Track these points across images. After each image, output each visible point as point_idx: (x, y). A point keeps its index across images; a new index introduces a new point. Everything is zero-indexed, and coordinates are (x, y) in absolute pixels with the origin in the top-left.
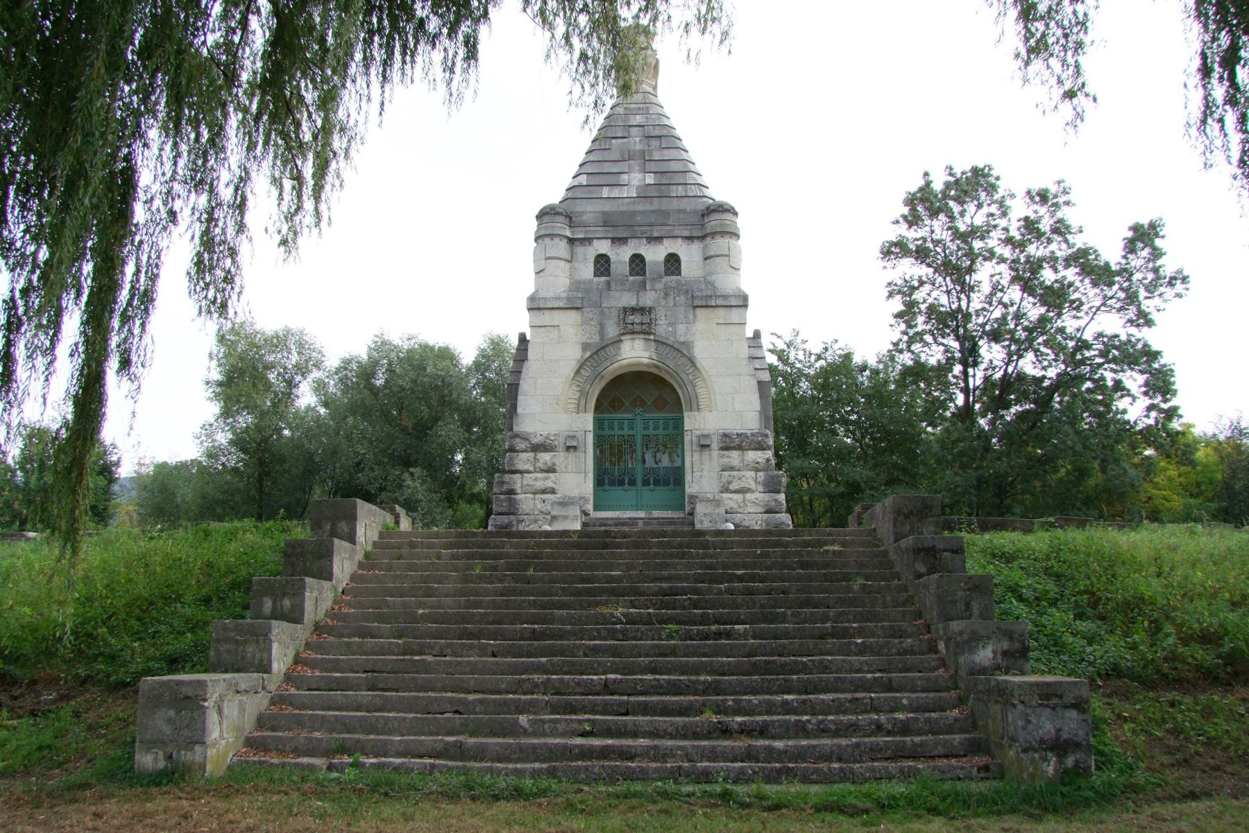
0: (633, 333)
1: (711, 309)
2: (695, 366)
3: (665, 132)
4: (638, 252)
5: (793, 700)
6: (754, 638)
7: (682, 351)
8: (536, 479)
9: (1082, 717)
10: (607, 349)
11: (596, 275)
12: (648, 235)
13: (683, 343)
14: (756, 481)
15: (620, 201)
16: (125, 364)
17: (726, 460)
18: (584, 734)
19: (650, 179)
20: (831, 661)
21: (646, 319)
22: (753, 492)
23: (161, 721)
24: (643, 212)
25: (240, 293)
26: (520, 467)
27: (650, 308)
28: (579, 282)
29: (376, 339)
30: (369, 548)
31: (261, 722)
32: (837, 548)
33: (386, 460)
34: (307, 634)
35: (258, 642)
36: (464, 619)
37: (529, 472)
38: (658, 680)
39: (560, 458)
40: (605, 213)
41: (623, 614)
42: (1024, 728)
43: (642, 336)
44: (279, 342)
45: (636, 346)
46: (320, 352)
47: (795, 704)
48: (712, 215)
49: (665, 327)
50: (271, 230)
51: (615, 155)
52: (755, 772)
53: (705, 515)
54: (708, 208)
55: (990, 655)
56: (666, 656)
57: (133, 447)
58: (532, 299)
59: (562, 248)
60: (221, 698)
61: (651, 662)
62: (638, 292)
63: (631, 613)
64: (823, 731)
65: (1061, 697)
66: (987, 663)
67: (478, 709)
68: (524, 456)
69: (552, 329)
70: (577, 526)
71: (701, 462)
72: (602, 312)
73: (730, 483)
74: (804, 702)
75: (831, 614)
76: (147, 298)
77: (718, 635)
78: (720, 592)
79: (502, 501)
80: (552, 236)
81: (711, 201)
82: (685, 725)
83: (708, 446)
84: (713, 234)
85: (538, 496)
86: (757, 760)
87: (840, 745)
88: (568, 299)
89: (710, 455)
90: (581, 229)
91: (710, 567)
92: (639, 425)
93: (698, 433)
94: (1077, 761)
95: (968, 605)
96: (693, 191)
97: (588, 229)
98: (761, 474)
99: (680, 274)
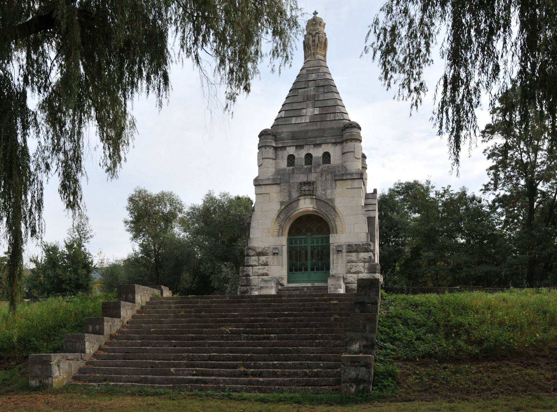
0: (305, 195)
1: (344, 181)
2: (336, 212)
3: (327, 83)
6: (278, 340)
7: (329, 204)
8: (259, 269)
9: (367, 370)
11: (288, 166)
12: (314, 143)
13: (330, 199)
14: (364, 268)
15: (301, 125)
16: (34, 232)
17: (350, 258)
18: (194, 375)
19: (317, 111)
21: (311, 188)
22: (362, 273)
23: (37, 369)
24: (312, 130)
25: (81, 199)
26: (252, 263)
27: (313, 182)
28: (280, 170)
29: (208, 196)
30: (144, 304)
31: (81, 370)
32: (335, 302)
34: (107, 339)
35: (80, 342)
36: (169, 332)
37: (256, 266)
38: (229, 355)
39: (270, 259)
41: (230, 330)
42: (343, 374)
43: (309, 197)
44: (161, 198)
45: (306, 202)
46: (181, 204)
47: (278, 365)
49: (321, 191)
50: (102, 164)
51: (300, 99)
53: (332, 285)
55: (358, 347)
57: (98, 254)
58: (256, 180)
59: (270, 152)
60: (59, 361)
62: (307, 174)
63: (233, 330)
64: (283, 375)
65: (359, 362)
66: (356, 350)
68: (253, 258)
69: (266, 195)
70: (273, 292)
73: (351, 269)
74: (281, 364)
76: (39, 204)
77: (264, 338)
78: (275, 321)
79: (243, 280)
80: (265, 147)
81: (348, 121)
83: (341, 251)
84: (347, 141)
85: (260, 277)
86: (253, 385)
87: (284, 380)
88: (273, 179)
89: (342, 255)
91: (277, 311)
92: (309, 241)
93: (336, 244)
95: (364, 327)
96: (339, 116)
97: (285, 141)
98: (367, 264)
99: (330, 163)
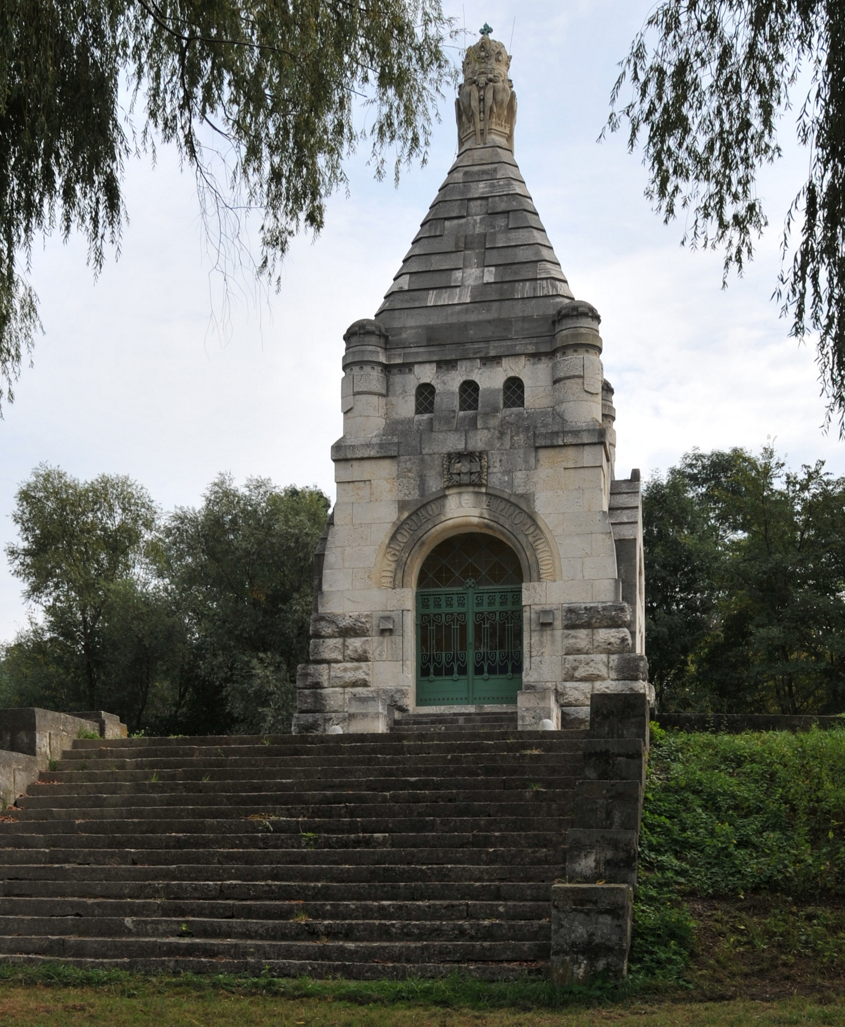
0: (460, 485)
1: (557, 450)
3: (514, 205)
4: (469, 378)
5: (390, 905)
8: (345, 670)
9: (616, 922)
10: (429, 508)
11: (418, 412)
12: (482, 355)
13: (521, 496)
14: (608, 666)
17: (572, 641)
18: (182, 935)
19: (489, 276)
20: (450, 870)
21: (475, 468)
22: (604, 679)
24: (478, 324)
26: (327, 655)
27: (481, 453)
28: (397, 422)
29: (217, 488)
30: (57, 758)
33: (232, 644)
36: (119, 828)
37: (337, 661)
38: (270, 886)
39: (373, 644)
40: (429, 328)
41: (272, 823)
42: (556, 932)
43: (471, 489)
45: (463, 502)
46: (149, 508)
47: (392, 910)
48: (564, 322)
49: (499, 475)
52: (314, 969)
53: (527, 709)
54: (559, 312)
55: (593, 864)
56: (297, 863)
59: (373, 378)
61: (273, 868)
62: (466, 432)
63: (280, 822)
65: (595, 903)
67: (96, 912)
68: (331, 642)
69: (362, 484)
70: (381, 727)
71: (541, 644)
72: (422, 460)
73: (575, 669)
75: (482, 822)
77: (357, 843)
79: (306, 696)
80: (361, 364)
82: (275, 927)
83: (550, 624)
84: (564, 349)
85: (349, 689)
86: (329, 959)
87: (409, 947)
88: (381, 446)
89: (552, 636)
90: (399, 351)
91: (390, 773)
92: (471, 599)
93: (538, 608)
94: (608, 964)
96: (545, 289)
98: (615, 657)
99: (522, 404)
